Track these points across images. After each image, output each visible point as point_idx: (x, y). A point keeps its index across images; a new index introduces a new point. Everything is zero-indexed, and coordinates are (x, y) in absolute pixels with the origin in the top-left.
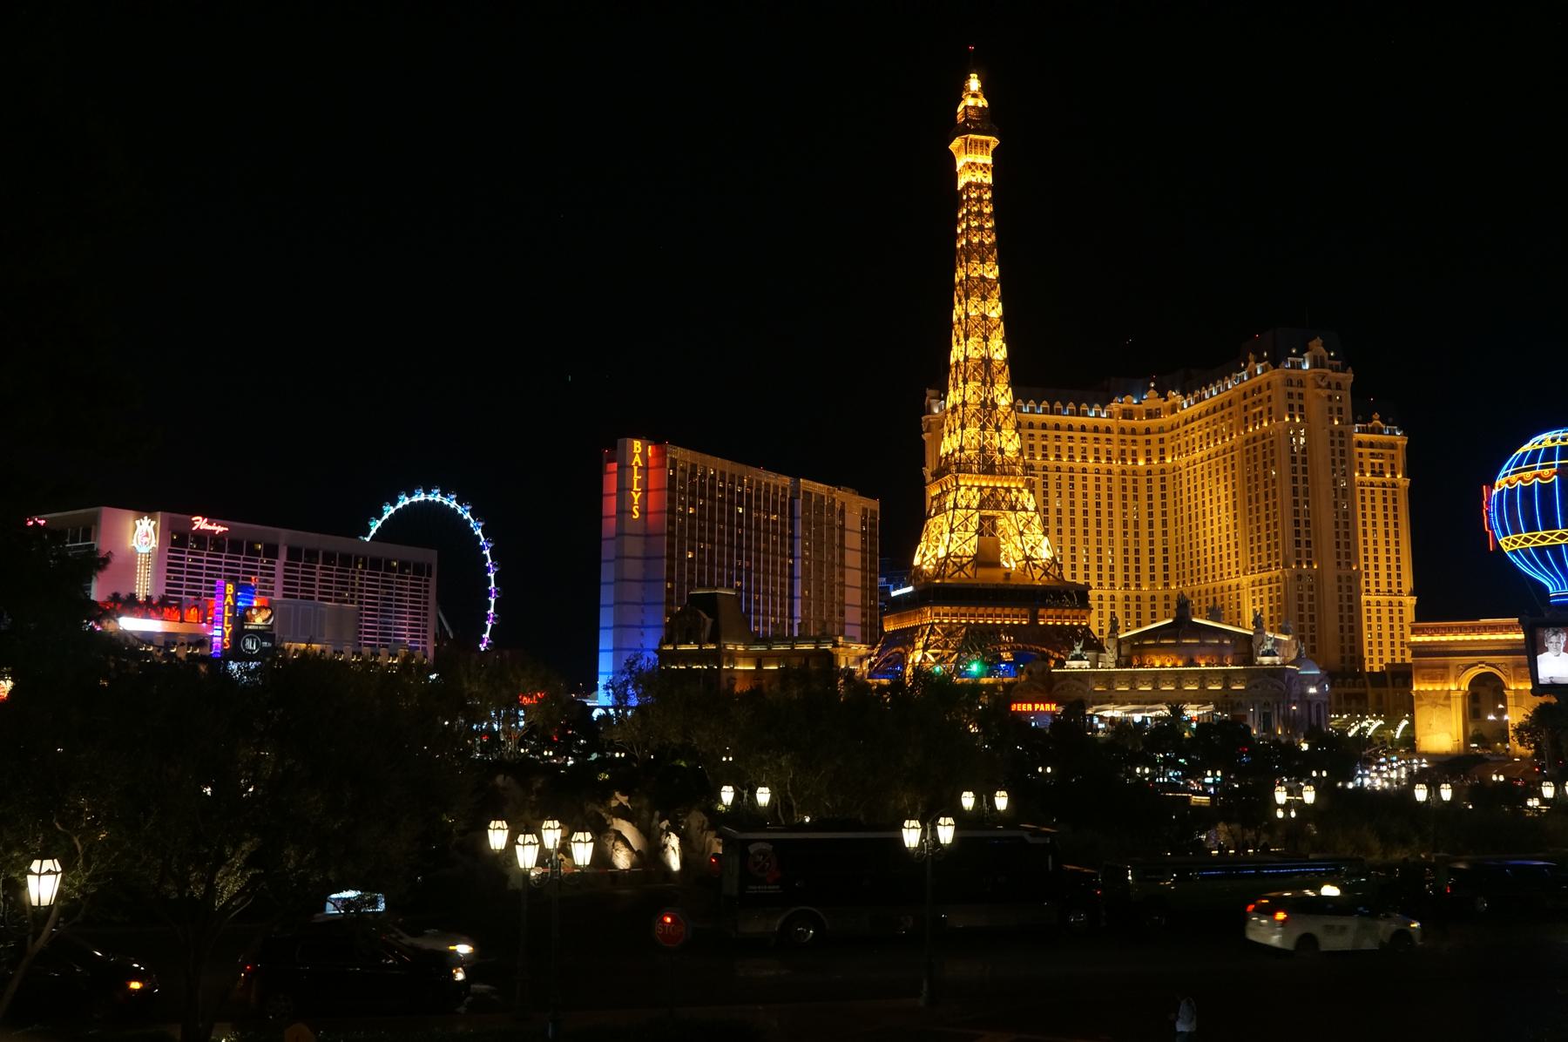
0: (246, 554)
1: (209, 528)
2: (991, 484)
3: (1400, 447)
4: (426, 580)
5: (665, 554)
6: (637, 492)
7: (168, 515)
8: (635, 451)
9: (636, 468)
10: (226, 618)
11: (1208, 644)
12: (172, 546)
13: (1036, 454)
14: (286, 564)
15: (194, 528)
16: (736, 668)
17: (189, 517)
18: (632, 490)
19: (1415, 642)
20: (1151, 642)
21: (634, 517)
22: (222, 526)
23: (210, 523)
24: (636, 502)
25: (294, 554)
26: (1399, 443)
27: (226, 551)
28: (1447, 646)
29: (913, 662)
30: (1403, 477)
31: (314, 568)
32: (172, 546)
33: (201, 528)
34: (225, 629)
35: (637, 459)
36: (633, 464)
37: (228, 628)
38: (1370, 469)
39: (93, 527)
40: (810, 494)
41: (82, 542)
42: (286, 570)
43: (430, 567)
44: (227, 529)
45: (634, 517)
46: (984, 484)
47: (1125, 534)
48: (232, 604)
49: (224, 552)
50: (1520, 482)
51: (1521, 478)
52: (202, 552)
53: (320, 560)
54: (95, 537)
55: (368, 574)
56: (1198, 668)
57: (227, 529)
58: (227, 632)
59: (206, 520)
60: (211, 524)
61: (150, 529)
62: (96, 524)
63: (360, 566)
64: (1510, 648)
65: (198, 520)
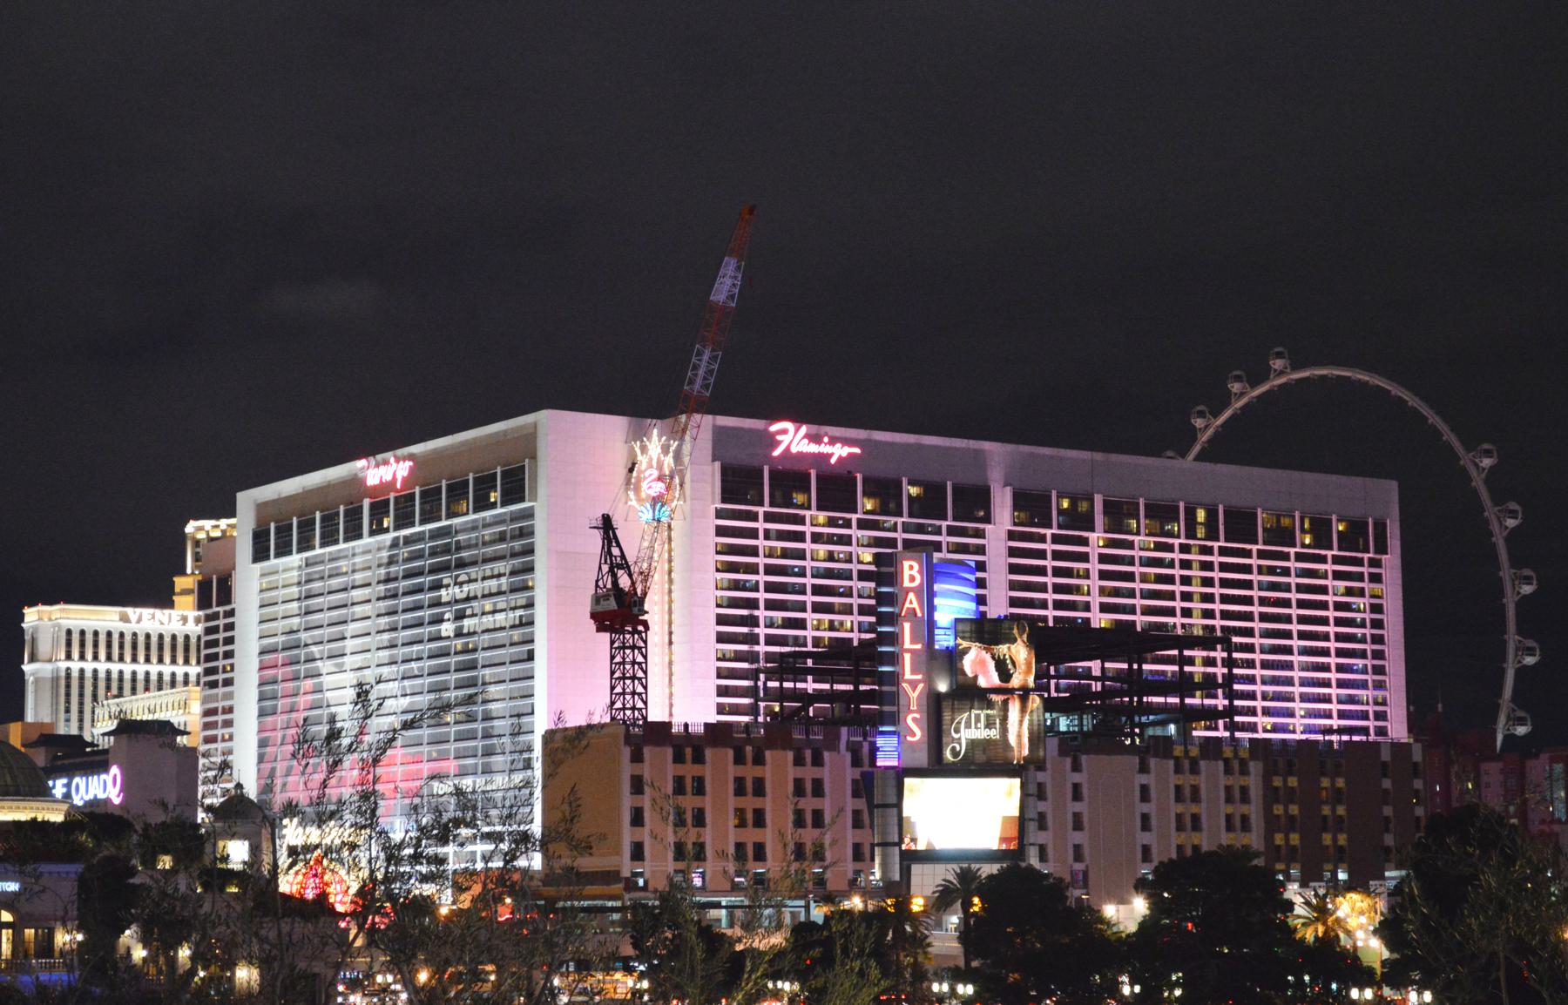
0: (772, 505)
1: (813, 448)
4: (1375, 563)
7: (704, 425)
12: (724, 501)
14: (1012, 536)
15: (776, 453)
16: (873, 585)
23: (814, 438)
25: (1031, 506)
27: (1260, 539)
31: (1084, 542)
32: (724, 501)
33: (794, 449)
37: (914, 685)
42: (1013, 552)
43: (1381, 527)
44: (857, 450)
53: (1099, 519)
57: (857, 450)
59: (804, 429)
62: (534, 457)
63: (1201, 532)
65: (785, 432)
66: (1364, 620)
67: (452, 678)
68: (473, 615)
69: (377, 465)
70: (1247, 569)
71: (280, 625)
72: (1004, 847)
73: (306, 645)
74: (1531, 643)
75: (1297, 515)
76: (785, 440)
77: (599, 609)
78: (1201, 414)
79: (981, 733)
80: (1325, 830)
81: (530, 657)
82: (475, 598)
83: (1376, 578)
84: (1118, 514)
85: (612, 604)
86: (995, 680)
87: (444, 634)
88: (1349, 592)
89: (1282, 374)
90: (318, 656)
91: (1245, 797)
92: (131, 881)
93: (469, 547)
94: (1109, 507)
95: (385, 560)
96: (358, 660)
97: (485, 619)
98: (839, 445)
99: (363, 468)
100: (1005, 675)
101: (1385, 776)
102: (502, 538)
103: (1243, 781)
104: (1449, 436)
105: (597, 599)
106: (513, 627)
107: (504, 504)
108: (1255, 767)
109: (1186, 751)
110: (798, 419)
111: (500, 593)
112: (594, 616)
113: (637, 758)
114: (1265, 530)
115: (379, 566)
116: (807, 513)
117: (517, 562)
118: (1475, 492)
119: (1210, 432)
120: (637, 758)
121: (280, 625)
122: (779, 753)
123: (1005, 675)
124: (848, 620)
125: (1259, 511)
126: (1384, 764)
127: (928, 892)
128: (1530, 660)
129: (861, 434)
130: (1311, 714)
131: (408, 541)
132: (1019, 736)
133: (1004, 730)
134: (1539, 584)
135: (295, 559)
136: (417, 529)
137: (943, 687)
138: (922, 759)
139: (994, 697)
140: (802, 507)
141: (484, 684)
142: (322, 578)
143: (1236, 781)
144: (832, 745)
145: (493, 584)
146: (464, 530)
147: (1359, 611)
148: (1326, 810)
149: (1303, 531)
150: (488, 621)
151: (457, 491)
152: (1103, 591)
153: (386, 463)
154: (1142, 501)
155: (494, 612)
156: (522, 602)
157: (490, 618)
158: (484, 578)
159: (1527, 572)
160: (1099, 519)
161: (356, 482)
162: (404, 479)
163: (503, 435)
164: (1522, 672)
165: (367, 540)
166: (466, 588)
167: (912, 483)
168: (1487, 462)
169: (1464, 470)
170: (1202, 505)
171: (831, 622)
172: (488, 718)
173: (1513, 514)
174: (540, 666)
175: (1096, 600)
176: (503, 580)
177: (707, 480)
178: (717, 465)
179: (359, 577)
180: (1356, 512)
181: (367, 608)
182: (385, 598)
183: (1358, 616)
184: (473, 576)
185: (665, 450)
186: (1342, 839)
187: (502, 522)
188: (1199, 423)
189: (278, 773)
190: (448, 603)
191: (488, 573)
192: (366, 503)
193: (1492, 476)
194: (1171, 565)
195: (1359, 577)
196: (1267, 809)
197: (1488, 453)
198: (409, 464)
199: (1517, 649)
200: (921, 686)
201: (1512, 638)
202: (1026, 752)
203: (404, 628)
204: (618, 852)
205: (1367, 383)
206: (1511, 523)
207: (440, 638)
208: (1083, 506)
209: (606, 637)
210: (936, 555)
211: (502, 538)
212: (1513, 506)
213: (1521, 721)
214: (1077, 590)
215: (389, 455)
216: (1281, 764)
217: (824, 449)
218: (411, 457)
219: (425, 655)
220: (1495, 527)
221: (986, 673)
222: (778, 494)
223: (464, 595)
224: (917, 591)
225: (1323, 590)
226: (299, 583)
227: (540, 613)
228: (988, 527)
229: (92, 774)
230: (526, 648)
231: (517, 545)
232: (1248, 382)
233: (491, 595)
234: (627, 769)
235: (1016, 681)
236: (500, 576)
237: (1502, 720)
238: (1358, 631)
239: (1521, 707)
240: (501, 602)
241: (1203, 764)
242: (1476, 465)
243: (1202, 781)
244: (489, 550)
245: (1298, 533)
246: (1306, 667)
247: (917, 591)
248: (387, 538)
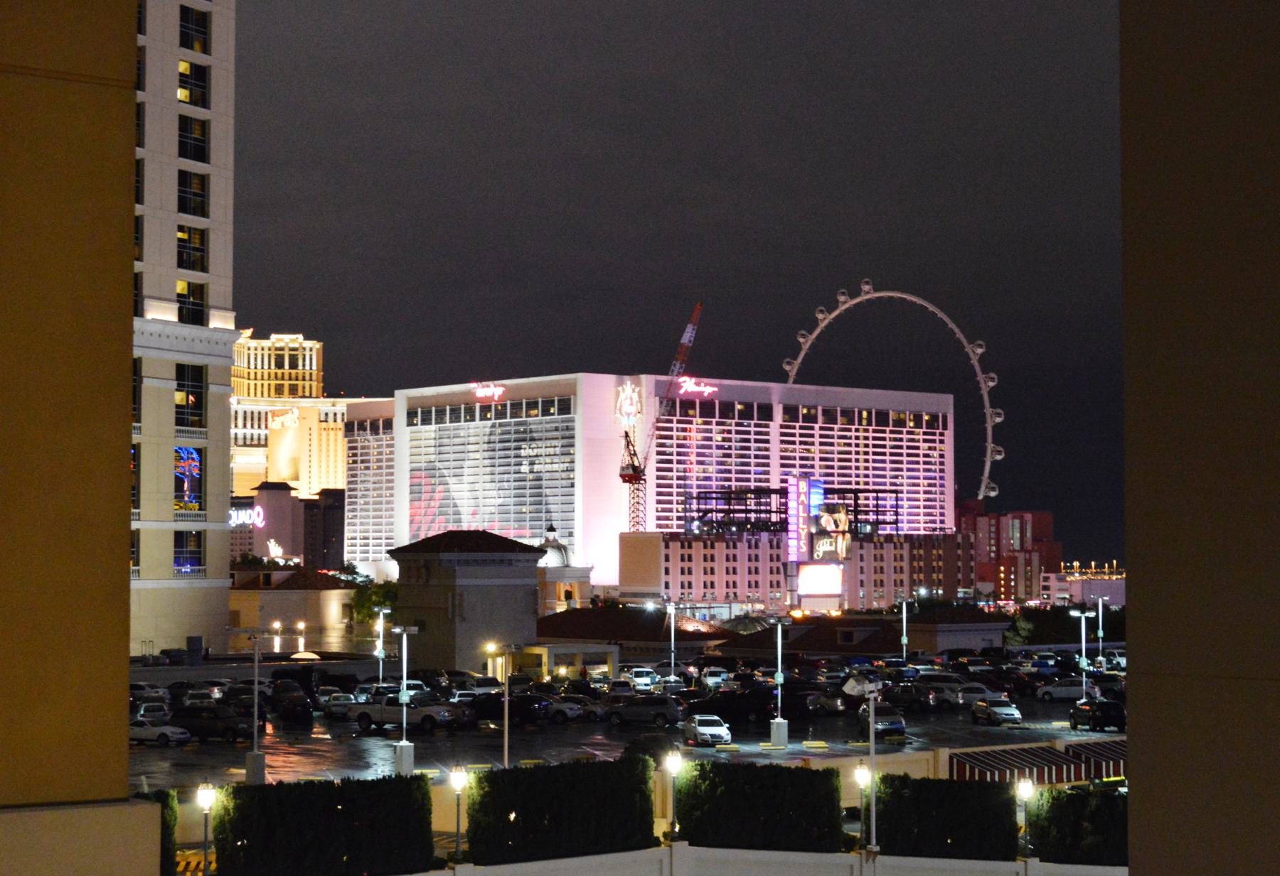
0: (681, 416)
1: (697, 389)
7: (647, 380)
10: (801, 519)
11: (991, 779)
14: (782, 427)
19: (241, 768)
22: (712, 385)
23: (698, 384)
25: (791, 412)
27: (839, 422)
29: (181, 733)
31: (812, 428)
34: (800, 530)
37: (803, 529)
39: (572, 397)
41: (511, 417)
42: (783, 434)
43: (945, 418)
44: (716, 389)
49: (888, 426)
52: (794, 424)
53: (820, 418)
54: (575, 408)
55: (875, 431)
57: (716, 389)
62: (575, 394)
63: (864, 422)
65: (685, 382)
66: (936, 462)
67: (528, 492)
68: (540, 464)
69: (483, 387)
70: (884, 439)
71: (423, 458)
72: (632, 530)
73: (439, 469)
74: (1000, 448)
75: (908, 413)
77: (624, 473)
78: (822, 311)
80: (934, 572)
81: (572, 486)
82: (541, 456)
83: (942, 442)
84: (830, 416)
85: (630, 471)
87: (522, 471)
88: (930, 448)
89: (868, 293)
90: (447, 475)
91: (902, 559)
93: (537, 432)
94: (825, 412)
95: (488, 433)
96: (472, 479)
97: (547, 466)
98: (708, 387)
99: (474, 388)
100: (837, 526)
101: (959, 548)
102: (557, 429)
103: (901, 552)
104: (960, 335)
105: (623, 469)
106: (563, 471)
107: (559, 414)
108: (906, 546)
109: (879, 540)
111: (555, 455)
112: (621, 476)
113: (667, 547)
114: (893, 420)
115: (484, 435)
116: (694, 419)
117: (565, 441)
118: (972, 366)
119: (826, 322)
120: (667, 547)
121: (423, 458)
122: (720, 544)
123: (837, 526)
124: (711, 468)
125: (891, 412)
126: (959, 544)
127: (807, 613)
128: (999, 457)
130: (911, 507)
131: (501, 425)
132: (842, 549)
133: (836, 547)
134: (1005, 418)
135: (433, 427)
136: (508, 420)
137: (813, 530)
138: (806, 558)
139: (832, 534)
140: (692, 416)
141: (546, 496)
142: (449, 438)
143: (898, 552)
144: (740, 540)
145: (551, 451)
146: (535, 424)
147: (934, 457)
148: (935, 564)
149: (910, 420)
150: (549, 467)
151: (532, 405)
152: (821, 452)
153: (488, 386)
154: (839, 409)
155: (552, 463)
156: (569, 460)
157: (550, 465)
158: (546, 447)
159: (999, 411)
160: (820, 418)
161: (471, 394)
162: (499, 396)
163: (558, 382)
164: (994, 463)
165: (478, 423)
166: (536, 451)
167: (740, 403)
168: (980, 351)
169: (967, 354)
170: (865, 410)
171: (704, 469)
172: (548, 512)
173: (992, 379)
174: (578, 490)
175: (817, 456)
176: (557, 449)
177: (653, 408)
178: (657, 398)
179: (472, 440)
180: (933, 410)
181: (477, 456)
182: (488, 451)
183: (933, 460)
184: (540, 445)
185: (634, 391)
186: (941, 576)
187: (557, 422)
188: (820, 316)
189: (423, 529)
190: (526, 457)
191: (549, 445)
192: (478, 406)
193: (982, 359)
194: (850, 438)
195: (934, 441)
196: (911, 564)
197: (980, 346)
198: (504, 389)
199: (992, 451)
201: (990, 446)
202: (844, 555)
203: (499, 466)
204: (659, 585)
205: (915, 302)
206: (991, 384)
207: (520, 473)
208: (813, 411)
209: (627, 485)
210: (812, 478)
211: (557, 429)
212: (993, 375)
213: (993, 489)
214: (808, 451)
215: (490, 383)
216: (917, 545)
218: (503, 386)
219: (512, 480)
220: (982, 385)
221: (830, 525)
222: (683, 412)
223: (535, 454)
224: (805, 493)
225: (918, 448)
226: (435, 439)
227: (578, 466)
228: (771, 423)
229: (241, 509)
230: (570, 481)
231: (567, 433)
232: (849, 296)
233: (550, 455)
234: (663, 551)
236: (555, 447)
237: (983, 487)
238: (933, 467)
239: (994, 482)
240: (556, 459)
241: (885, 545)
242: (973, 351)
243: (884, 552)
244: (550, 435)
245: (908, 421)
246: (909, 485)
247: (805, 493)
248: (489, 423)
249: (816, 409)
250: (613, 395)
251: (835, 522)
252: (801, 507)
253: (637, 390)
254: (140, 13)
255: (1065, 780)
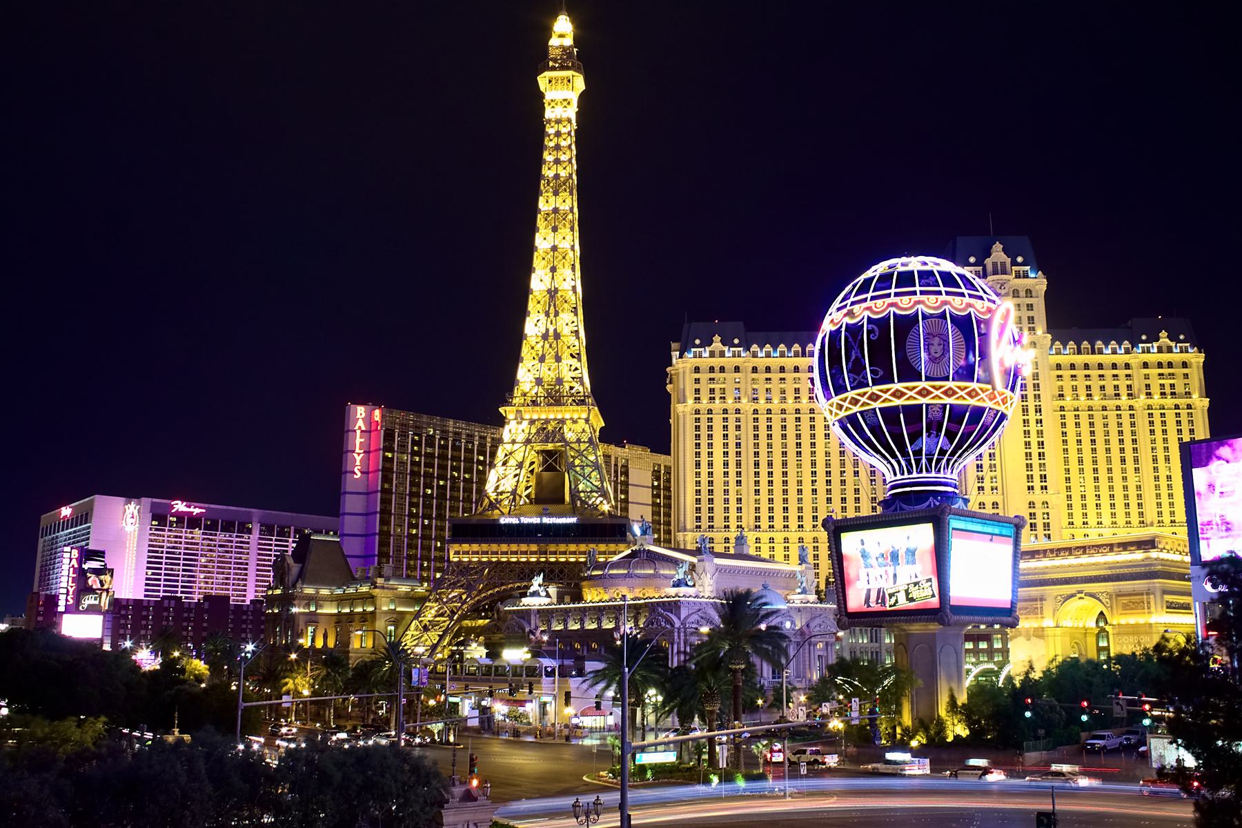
1: (188, 510)
2: (543, 416)
3: (1195, 366)
5: (378, 510)
6: (359, 454)
7: (147, 501)
8: (358, 416)
9: (358, 432)
10: (70, 579)
13: (760, 398)
16: (318, 611)
17: (168, 501)
18: (354, 452)
20: (600, 573)
21: (355, 477)
22: (200, 508)
24: (358, 463)
26: (1193, 360)
28: (1043, 573)
30: (1201, 396)
31: (287, 541)
34: (69, 588)
35: (360, 423)
36: (356, 428)
37: (72, 587)
38: (1159, 391)
40: (610, 457)
44: (204, 511)
45: (355, 477)
46: (535, 417)
47: (842, 473)
48: (76, 566)
50: (867, 313)
51: (869, 308)
56: (515, 608)
57: (204, 511)
58: (71, 590)
59: (185, 503)
60: (189, 507)
61: (136, 512)
62: (92, 510)
64: (1109, 572)
76: (176, 507)
79: (92, 602)
86: (99, 586)
92: (697, 716)
100: (102, 585)
110: (183, 501)
123: (102, 585)
129: (206, 505)
160: (292, 535)
200: (362, 455)
202: (107, 608)
217: (191, 510)
235: (105, 587)
249: (290, 528)
250: (122, 512)
251: (101, 582)
252: (71, 570)
253: (138, 507)
254: (1080, 822)
255: (948, 407)
